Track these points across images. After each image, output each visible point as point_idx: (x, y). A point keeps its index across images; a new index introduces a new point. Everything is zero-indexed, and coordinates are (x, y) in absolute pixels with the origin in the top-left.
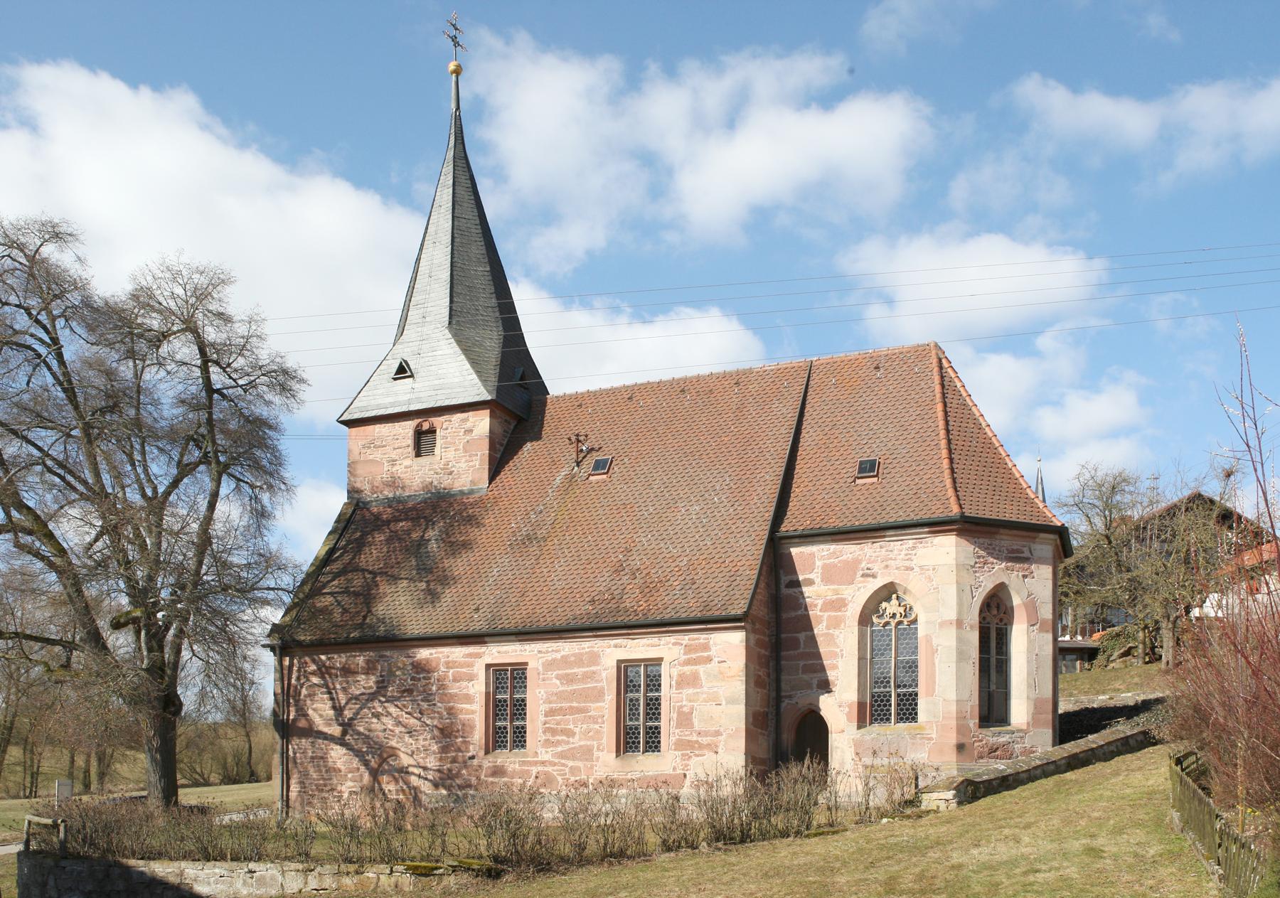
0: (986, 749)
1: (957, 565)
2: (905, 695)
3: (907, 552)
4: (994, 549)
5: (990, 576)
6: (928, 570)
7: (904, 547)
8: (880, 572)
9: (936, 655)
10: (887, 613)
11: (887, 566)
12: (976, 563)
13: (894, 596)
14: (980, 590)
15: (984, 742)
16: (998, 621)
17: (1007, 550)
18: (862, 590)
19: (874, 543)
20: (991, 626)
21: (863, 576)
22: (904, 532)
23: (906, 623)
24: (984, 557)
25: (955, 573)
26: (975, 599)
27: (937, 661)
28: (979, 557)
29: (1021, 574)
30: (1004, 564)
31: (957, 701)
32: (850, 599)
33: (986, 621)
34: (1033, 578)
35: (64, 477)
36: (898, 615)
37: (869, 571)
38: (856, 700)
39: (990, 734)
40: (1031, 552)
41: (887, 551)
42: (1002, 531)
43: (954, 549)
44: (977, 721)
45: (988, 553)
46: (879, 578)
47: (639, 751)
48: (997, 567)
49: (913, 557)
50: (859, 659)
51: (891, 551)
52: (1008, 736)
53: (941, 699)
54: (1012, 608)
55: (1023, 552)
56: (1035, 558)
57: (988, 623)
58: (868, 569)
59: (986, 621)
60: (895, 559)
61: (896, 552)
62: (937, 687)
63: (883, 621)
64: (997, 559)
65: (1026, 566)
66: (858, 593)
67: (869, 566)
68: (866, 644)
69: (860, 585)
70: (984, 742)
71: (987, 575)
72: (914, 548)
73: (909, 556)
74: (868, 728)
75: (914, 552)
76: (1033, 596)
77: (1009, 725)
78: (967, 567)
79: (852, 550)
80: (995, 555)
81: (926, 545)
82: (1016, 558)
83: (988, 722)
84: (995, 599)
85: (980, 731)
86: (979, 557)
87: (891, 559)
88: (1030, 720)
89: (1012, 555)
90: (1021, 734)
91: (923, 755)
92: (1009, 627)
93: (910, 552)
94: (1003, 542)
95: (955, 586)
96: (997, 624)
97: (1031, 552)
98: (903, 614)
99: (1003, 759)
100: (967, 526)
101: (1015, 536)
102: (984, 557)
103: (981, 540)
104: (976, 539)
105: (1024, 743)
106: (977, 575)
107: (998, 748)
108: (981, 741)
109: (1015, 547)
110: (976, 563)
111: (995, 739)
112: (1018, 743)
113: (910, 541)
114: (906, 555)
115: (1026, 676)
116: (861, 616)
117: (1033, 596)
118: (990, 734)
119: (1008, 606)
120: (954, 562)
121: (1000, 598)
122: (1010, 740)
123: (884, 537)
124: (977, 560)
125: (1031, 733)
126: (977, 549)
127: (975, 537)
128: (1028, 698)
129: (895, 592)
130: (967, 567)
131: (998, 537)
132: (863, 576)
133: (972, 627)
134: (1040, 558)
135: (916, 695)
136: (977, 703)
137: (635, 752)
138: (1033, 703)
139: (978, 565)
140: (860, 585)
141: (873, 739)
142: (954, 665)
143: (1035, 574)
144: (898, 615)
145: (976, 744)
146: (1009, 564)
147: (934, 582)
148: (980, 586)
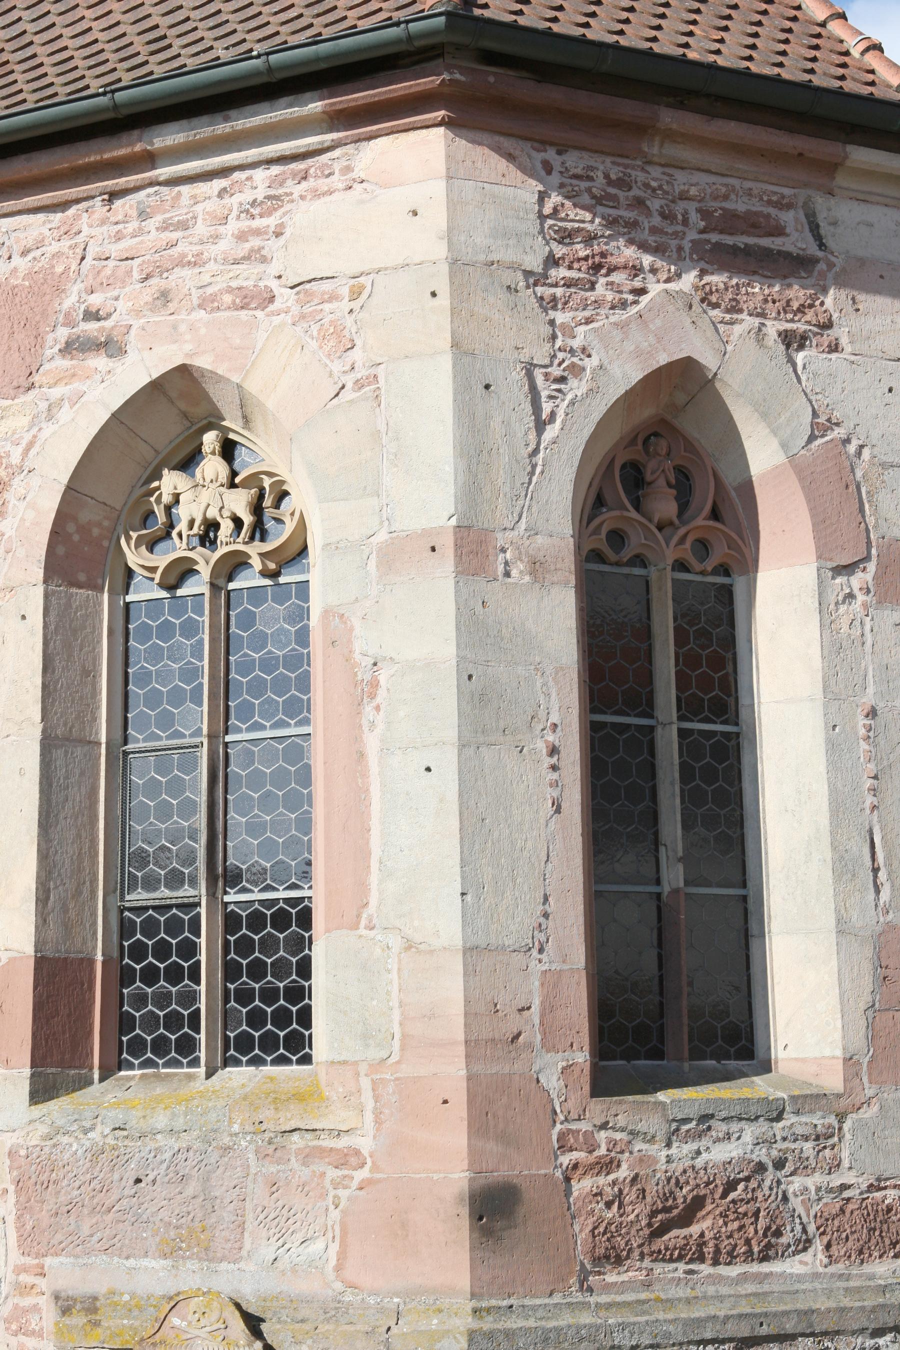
0: (637, 1212)
1: (454, 263)
2: (256, 921)
3: (245, 224)
4: (639, 203)
5: (622, 326)
6: (333, 297)
7: (234, 201)
8: (137, 324)
9: (368, 710)
10: (182, 526)
11: (164, 296)
12: (552, 261)
13: (210, 439)
14: (576, 387)
15: (623, 1173)
16: (686, 552)
17: (705, 214)
18: (64, 414)
19: (113, 196)
20: (653, 573)
21: (69, 348)
22: (222, 128)
23: (256, 563)
24: (589, 239)
25: (444, 300)
26: (551, 432)
27: (372, 743)
28: (566, 237)
29: (773, 328)
30: (689, 279)
31: (469, 951)
32: (15, 458)
33: (627, 554)
34: (834, 348)
35: (878, 869)
36: (227, 527)
37: (92, 327)
38: (30, 950)
39: (653, 1124)
40: (815, 228)
41: (165, 227)
42: (669, 118)
43: (439, 188)
44: (582, 1057)
45: (611, 222)
46: (132, 356)
47: (195, 1063)
48: (655, 289)
49: (272, 246)
50: (48, 744)
51: (183, 226)
52: (750, 1133)
53: (395, 942)
54: (747, 489)
55: (779, 231)
56: (839, 262)
57: (639, 560)
58: (92, 315)
59: (627, 554)
60: (197, 263)
61: (201, 229)
62: (374, 878)
63: (162, 559)
64: (658, 250)
65: (797, 293)
66: (49, 429)
67: (95, 300)
68: (89, 673)
69: (56, 393)
70: (623, 1173)
71: (607, 319)
72: (274, 201)
73: (255, 242)
74: (96, 1088)
75: (271, 222)
76: (838, 433)
77: (766, 1067)
78: (509, 277)
79: (28, 238)
80: (645, 235)
81: (323, 184)
82: (748, 251)
83: (658, 1054)
84: (662, 446)
85: (598, 1108)
86: (566, 237)
87: (181, 262)
88: (859, 1041)
89: (729, 240)
90: (819, 1120)
91: (318, 1246)
92: (739, 585)
93: (258, 223)
94: (681, 177)
95: (446, 363)
96: (681, 566)
97: (815, 228)
98: (248, 519)
99: (732, 1258)
100: (493, 76)
101: (739, 149)
102: (589, 239)
103: (575, 161)
104: (551, 154)
105: (835, 1166)
106: (561, 317)
107: (698, 1203)
108: (608, 1165)
109: (740, 206)
110: (552, 261)
111: (682, 1150)
112: (803, 1167)
113: (260, 175)
114: (242, 237)
115: (824, 821)
116: (57, 532)
117: (838, 433)
118: (653, 1124)
119: (730, 479)
120: (441, 251)
121: (690, 447)
122: (761, 1154)
123: (150, 160)
124: (559, 251)
125: (869, 1113)
126: (555, 199)
127: (543, 143)
128: (843, 928)
129: (213, 421)
130: (509, 277)
131: (653, 149)
132: (69, 348)
133: (536, 567)
134: (862, 262)
135: (305, 918)
136: (578, 956)
137: (176, 1063)
138: (869, 952)
139: (562, 272)
140: (56, 393)
141: (96, 1153)
142: (452, 755)
143: (841, 333)
144: (227, 527)
145: (582, 1186)
146: (717, 279)
147: (356, 355)
148: (576, 370)
